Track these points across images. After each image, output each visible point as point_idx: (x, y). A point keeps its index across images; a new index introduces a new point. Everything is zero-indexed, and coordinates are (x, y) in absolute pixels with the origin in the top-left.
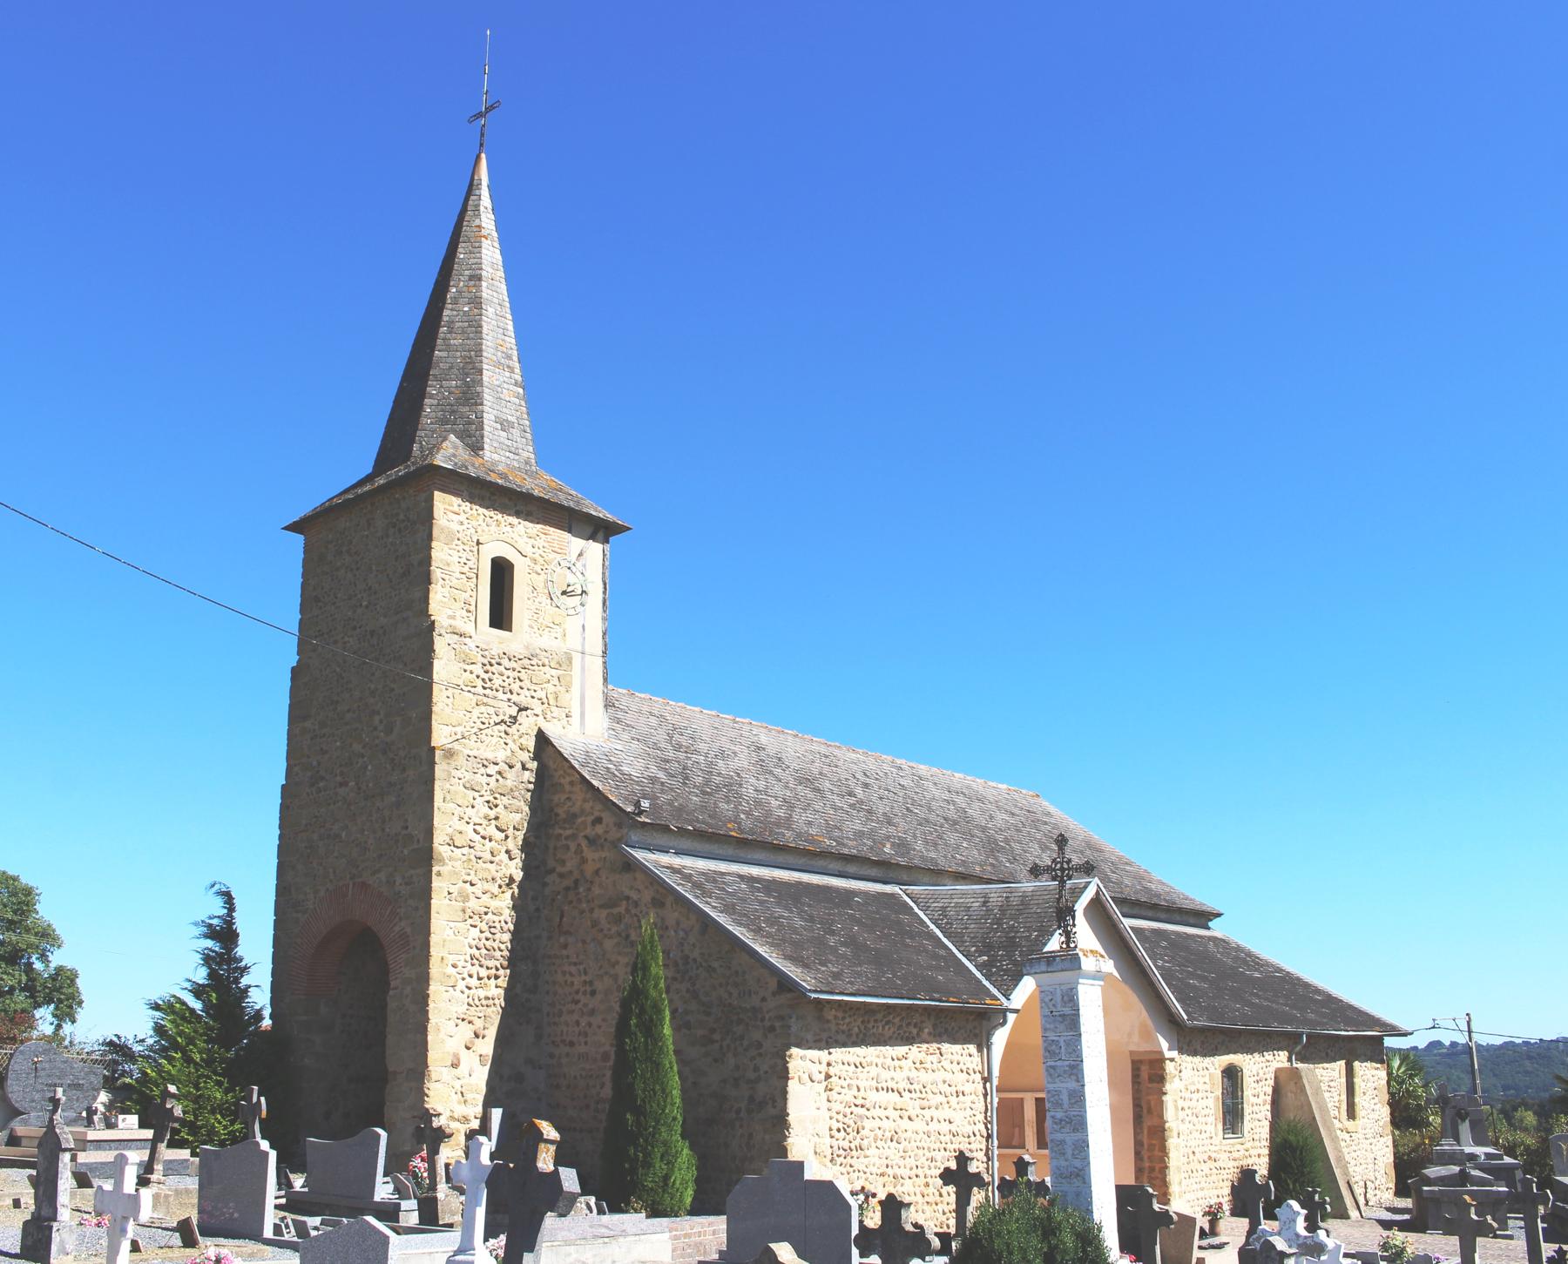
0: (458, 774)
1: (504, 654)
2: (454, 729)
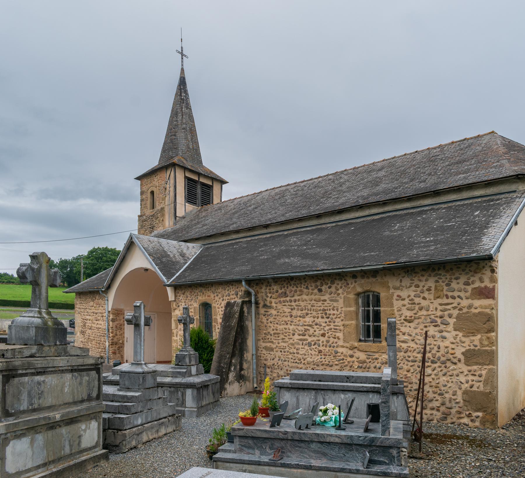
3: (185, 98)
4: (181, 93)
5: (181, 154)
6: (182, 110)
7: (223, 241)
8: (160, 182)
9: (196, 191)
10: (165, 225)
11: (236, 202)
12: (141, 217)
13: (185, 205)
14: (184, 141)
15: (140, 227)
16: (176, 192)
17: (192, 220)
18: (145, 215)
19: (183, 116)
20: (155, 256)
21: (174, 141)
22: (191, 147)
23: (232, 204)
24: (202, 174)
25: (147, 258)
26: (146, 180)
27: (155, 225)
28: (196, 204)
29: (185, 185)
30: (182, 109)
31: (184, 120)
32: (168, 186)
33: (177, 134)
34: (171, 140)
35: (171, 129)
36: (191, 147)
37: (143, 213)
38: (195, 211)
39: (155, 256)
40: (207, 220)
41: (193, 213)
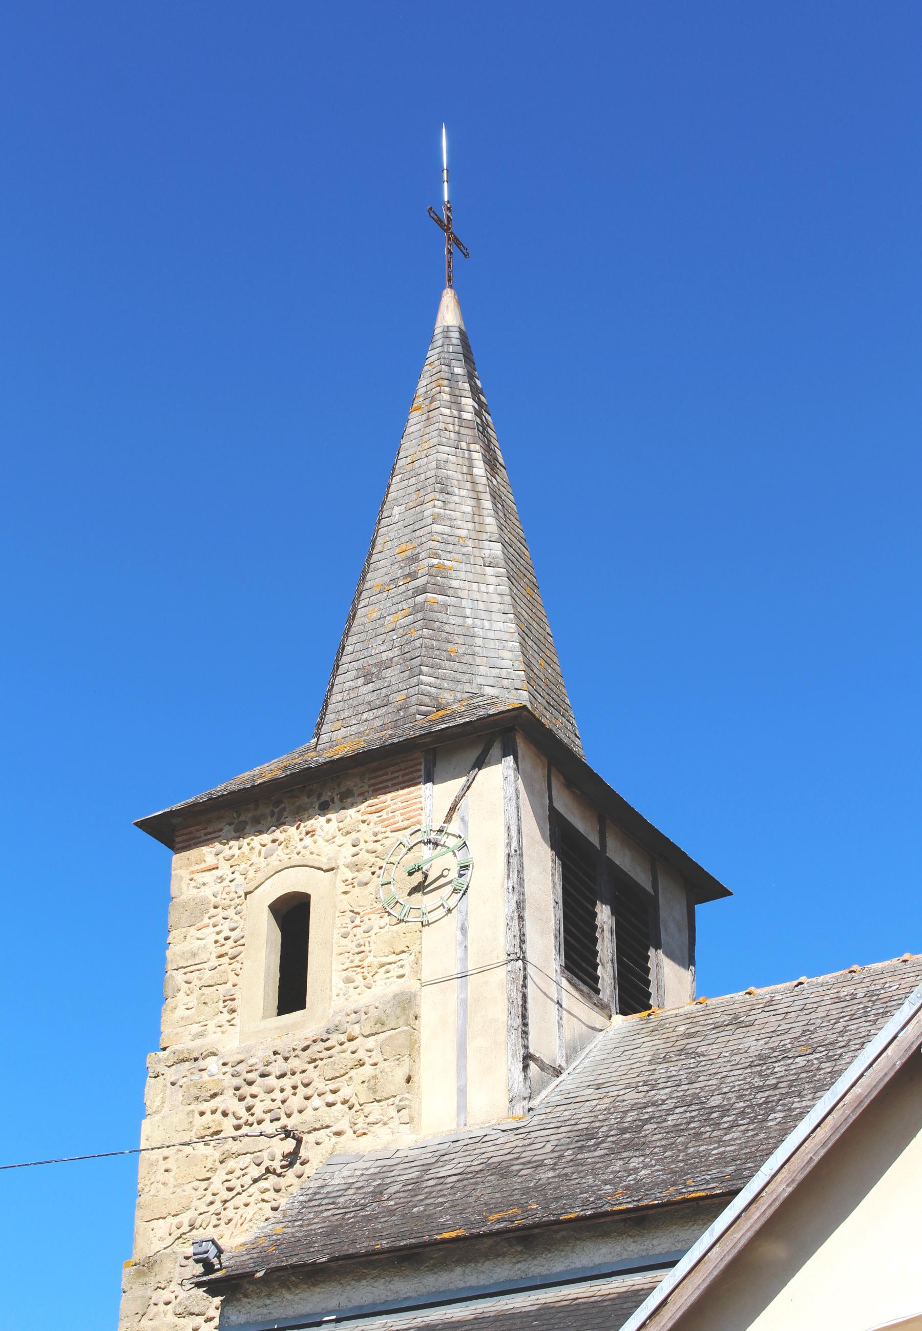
0: (166, 1295)
1: (275, 1053)
2: (176, 1220)
30: (471, 467)
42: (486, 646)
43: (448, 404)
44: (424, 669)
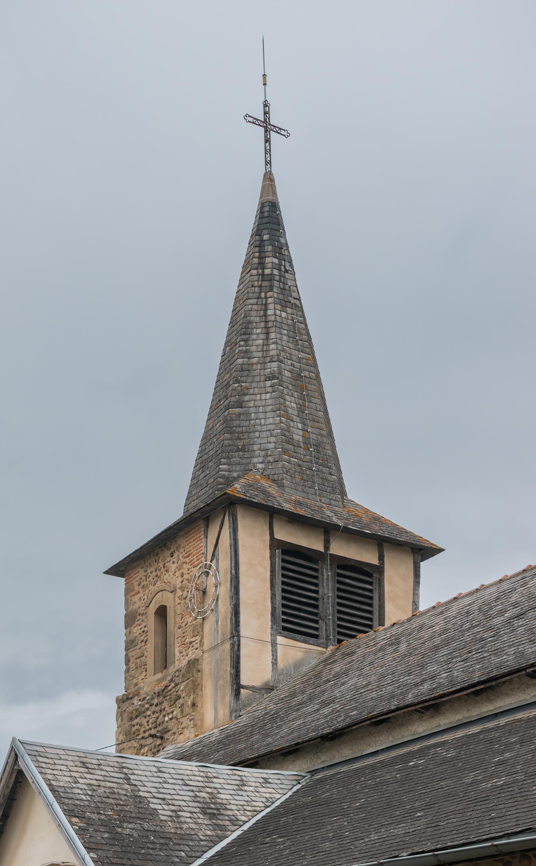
3: (276, 272)
4: (262, 258)
5: (260, 466)
6: (265, 315)
7: (382, 750)
8: (185, 571)
9: (316, 592)
10: (202, 721)
11: (455, 608)
12: (126, 704)
13: (274, 644)
14: (271, 420)
15: (121, 738)
16: (238, 599)
17: (293, 695)
18: (138, 694)
19: (268, 333)
20: (95, 816)
21: (236, 423)
22: (298, 437)
23: (439, 620)
24: (336, 527)
25: (60, 826)
26: (141, 573)
27: (171, 725)
28: (316, 637)
29: (273, 571)
30: (266, 310)
31: (273, 346)
32: (211, 580)
33: (247, 398)
34: (225, 421)
35: (228, 385)
36: (298, 437)
37: (133, 689)
38: (314, 662)
39: (95, 816)
40: (343, 684)
41: (304, 669)
42: (261, 436)
43: (256, 266)
44: (223, 460)
